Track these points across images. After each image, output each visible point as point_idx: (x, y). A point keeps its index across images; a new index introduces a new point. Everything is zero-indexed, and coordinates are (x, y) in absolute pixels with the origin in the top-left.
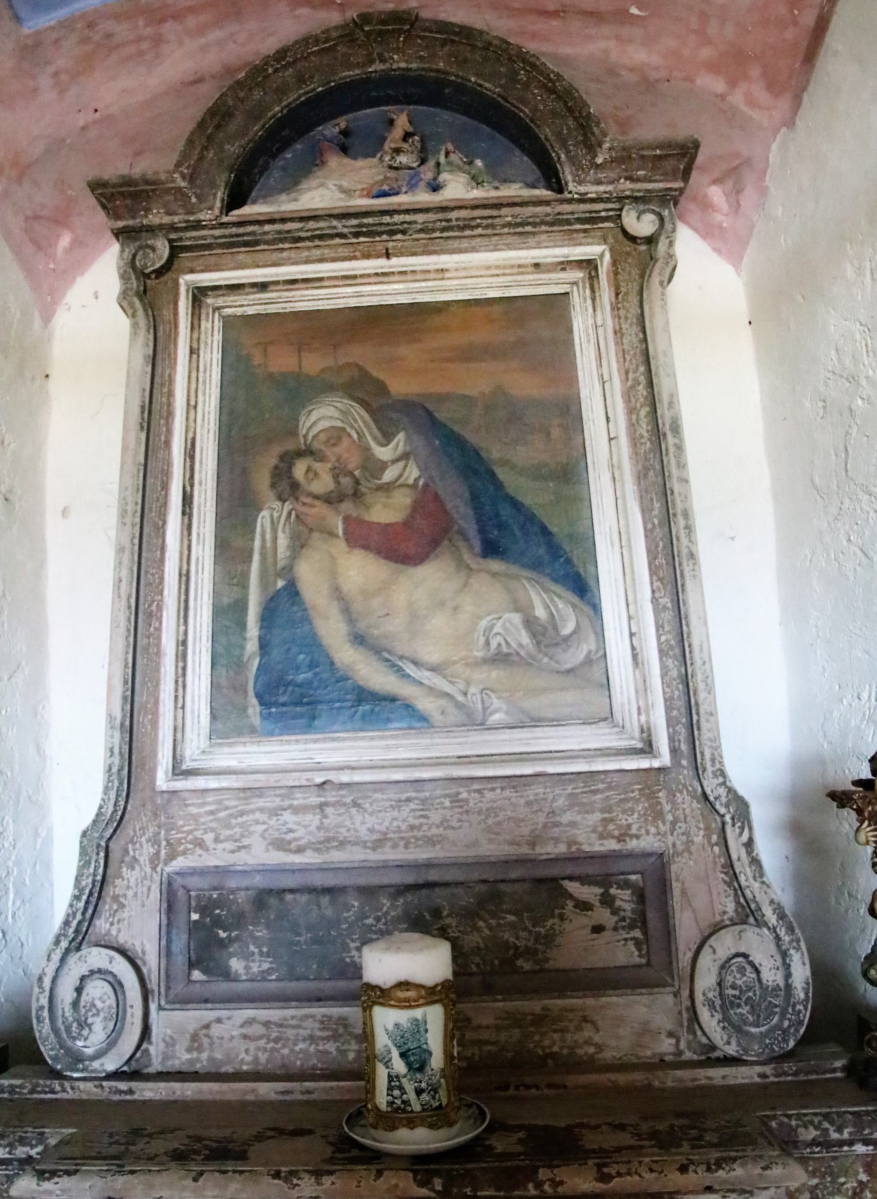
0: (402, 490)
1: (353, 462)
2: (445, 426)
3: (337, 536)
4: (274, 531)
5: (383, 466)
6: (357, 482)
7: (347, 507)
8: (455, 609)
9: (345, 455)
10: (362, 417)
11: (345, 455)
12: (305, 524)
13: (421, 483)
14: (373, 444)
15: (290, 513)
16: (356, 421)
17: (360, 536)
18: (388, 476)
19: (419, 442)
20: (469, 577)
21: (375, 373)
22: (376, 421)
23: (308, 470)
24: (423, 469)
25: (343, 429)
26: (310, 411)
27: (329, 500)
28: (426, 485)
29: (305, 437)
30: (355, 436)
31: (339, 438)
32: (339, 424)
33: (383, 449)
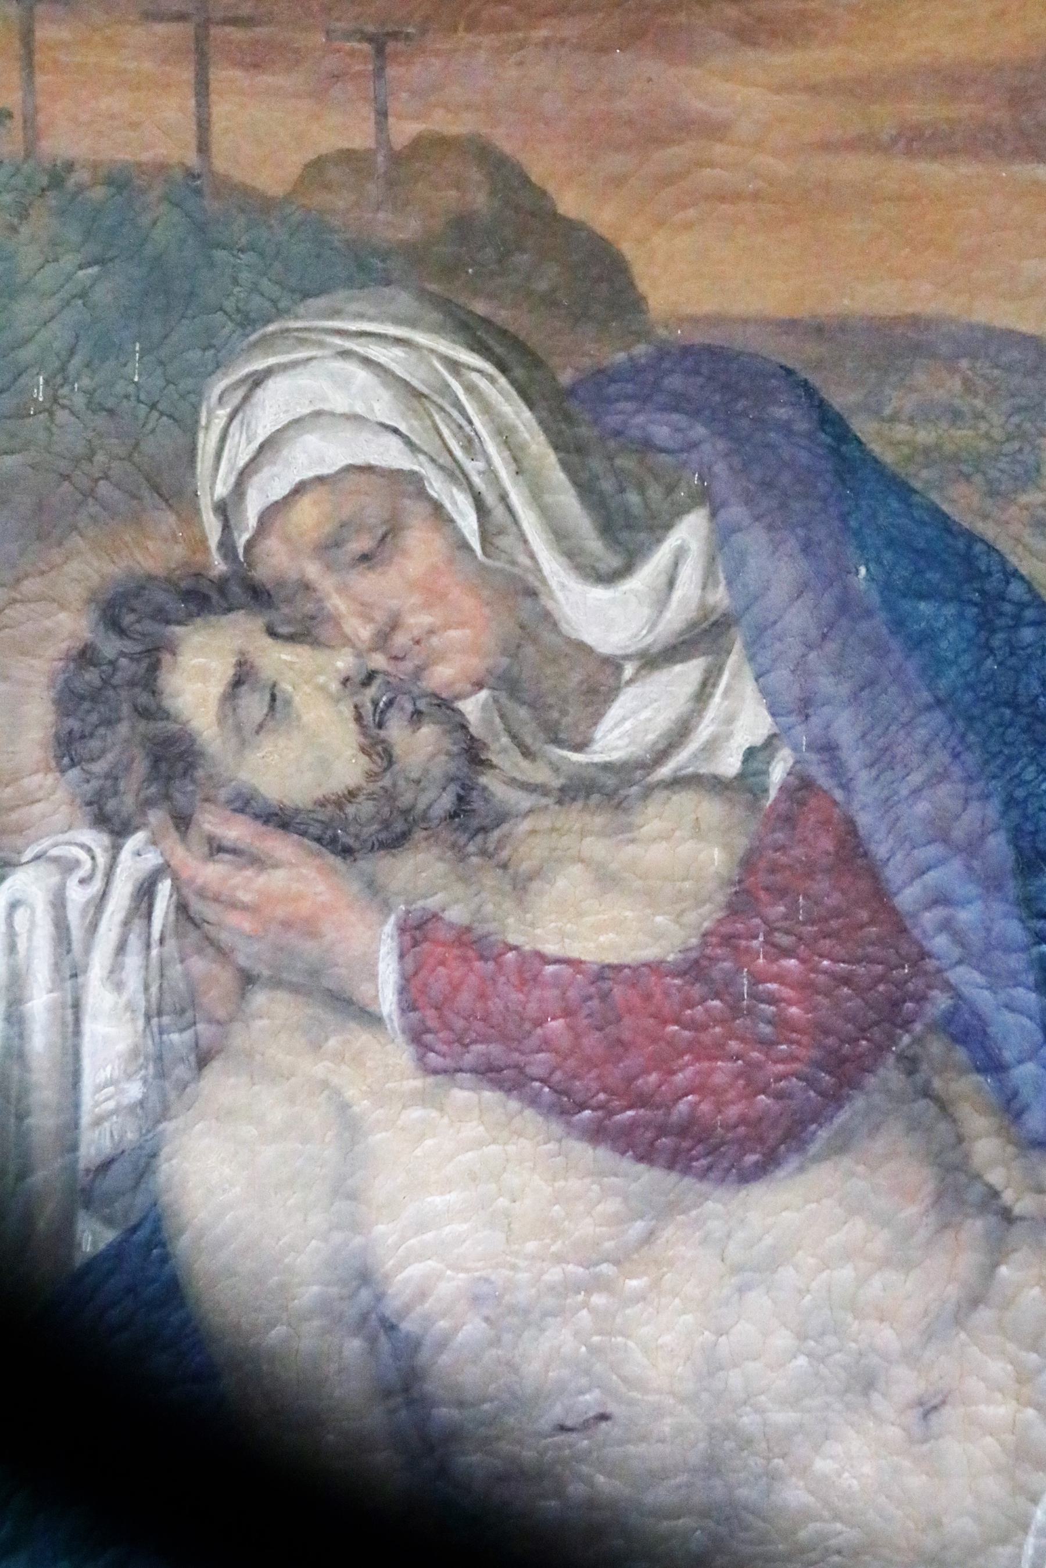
0: (684, 800)
1: (457, 652)
2: (903, 490)
3: (371, 1019)
4: (70, 971)
5: (601, 680)
6: (473, 754)
7: (420, 874)
8: (928, 1408)
9: (419, 621)
10: (505, 435)
11: (419, 621)
12: (223, 953)
13: (778, 773)
14: (552, 566)
15: (145, 892)
16: (471, 444)
17: (476, 1020)
18: (622, 730)
19: (776, 570)
20: (998, 1250)
21: (569, 203)
22: (570, 450)
23: (243, 677)
24: (794, 708)
25: (407, 484)
26: (257, 380)
27: (334, 832)
28: (801, 786)
29: (222, 509)
30: (468, 523)
31: (391, 533)
32: (391, 455)
33: (599, 593)
